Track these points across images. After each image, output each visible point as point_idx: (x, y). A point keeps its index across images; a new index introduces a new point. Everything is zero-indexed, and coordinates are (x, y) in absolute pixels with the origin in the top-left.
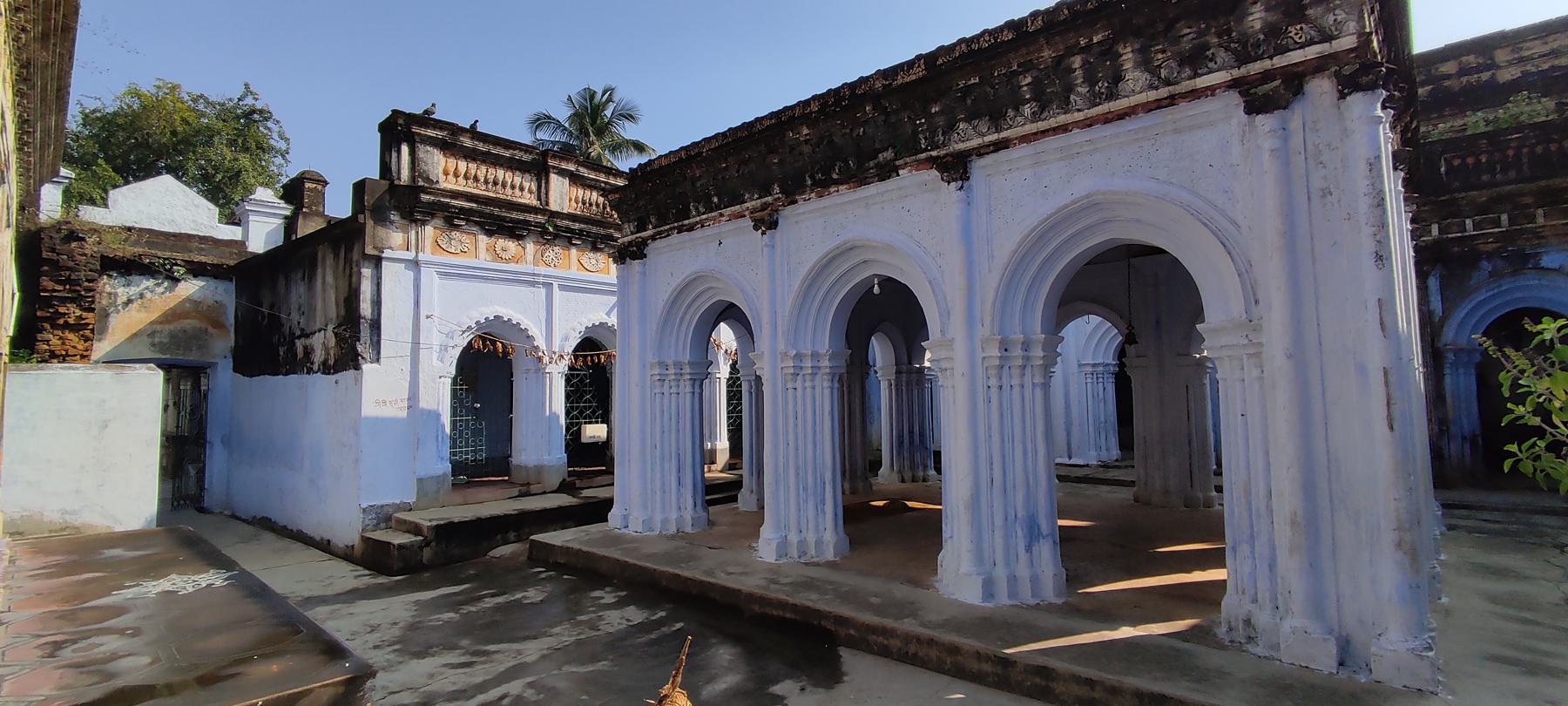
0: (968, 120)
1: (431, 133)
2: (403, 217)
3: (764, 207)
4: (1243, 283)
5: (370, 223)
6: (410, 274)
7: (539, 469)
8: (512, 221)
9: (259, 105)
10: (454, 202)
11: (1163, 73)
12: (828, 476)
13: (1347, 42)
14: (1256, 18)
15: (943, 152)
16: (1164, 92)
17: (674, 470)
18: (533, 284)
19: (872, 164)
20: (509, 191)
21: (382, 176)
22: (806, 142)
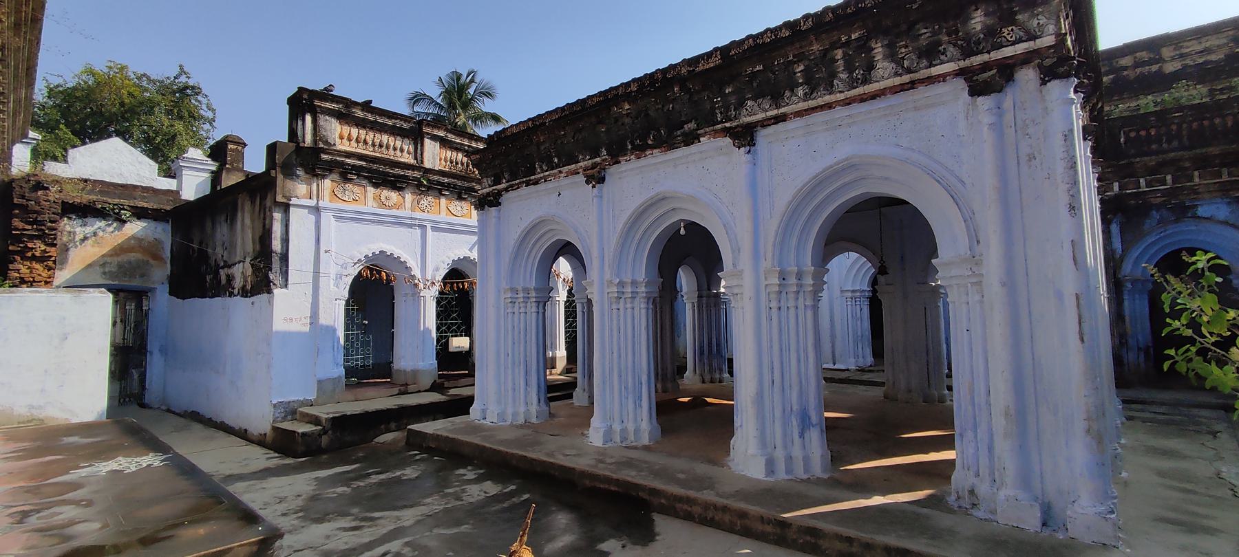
0: (754, 99)
1: (329, 105)
4: (967, 227)
5: (280, 177)
6: (313, 218)
7: (415, 373)
8: (394, 176)
10: (348, 161)
11: (906, 63)
12: (644, 378)
13: (1048, 40)
14: (978, 21)
15: (734, 124)
16: (906, 78)
17: (522, 373)
18: (411, 226)
19: (679, 133)
20: (391, 152)
21: (290, 140)
22: (628, 115)
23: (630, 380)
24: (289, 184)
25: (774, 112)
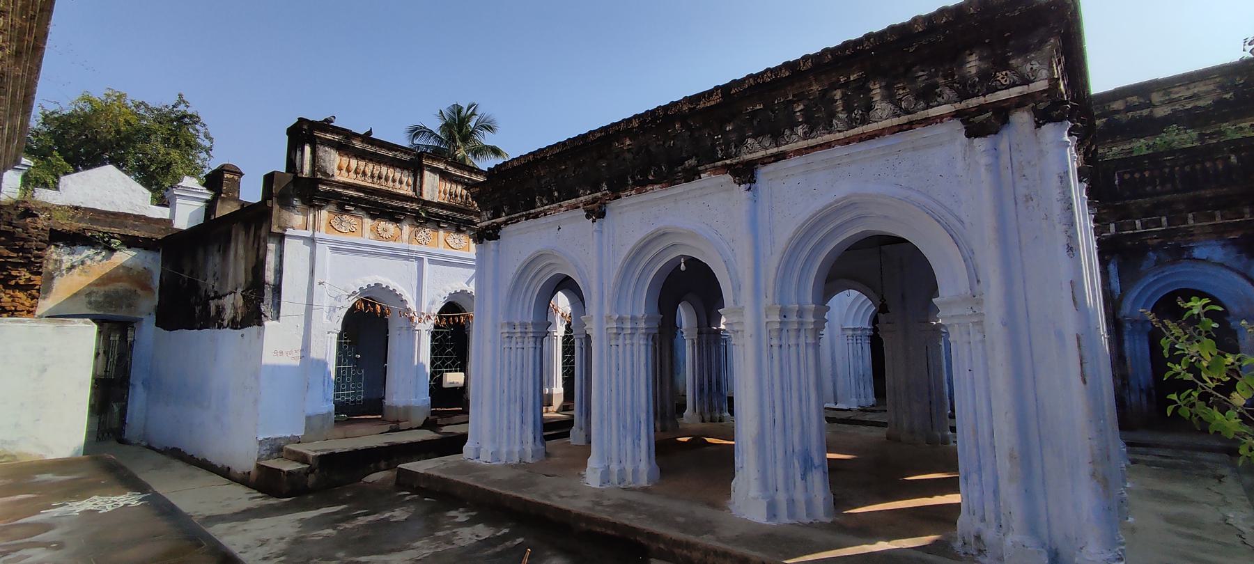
0: (755, 137)
1: (329, 136)
2: (303, 203)
3: (595, 200)
5: (276, 207)
6: (308, 249)
7: (408, 409)
8: (392, 207)
9: (189, 111)
10: (346, 192)
14: (973, 65)
16: (904, 119)
17: (518, 410)
18: (407, 258)
20: (390, 184)
21: (288, 170)
22: (629, 150)
23: (628, 419)
24: (285, 214)
25: (775, 150)
